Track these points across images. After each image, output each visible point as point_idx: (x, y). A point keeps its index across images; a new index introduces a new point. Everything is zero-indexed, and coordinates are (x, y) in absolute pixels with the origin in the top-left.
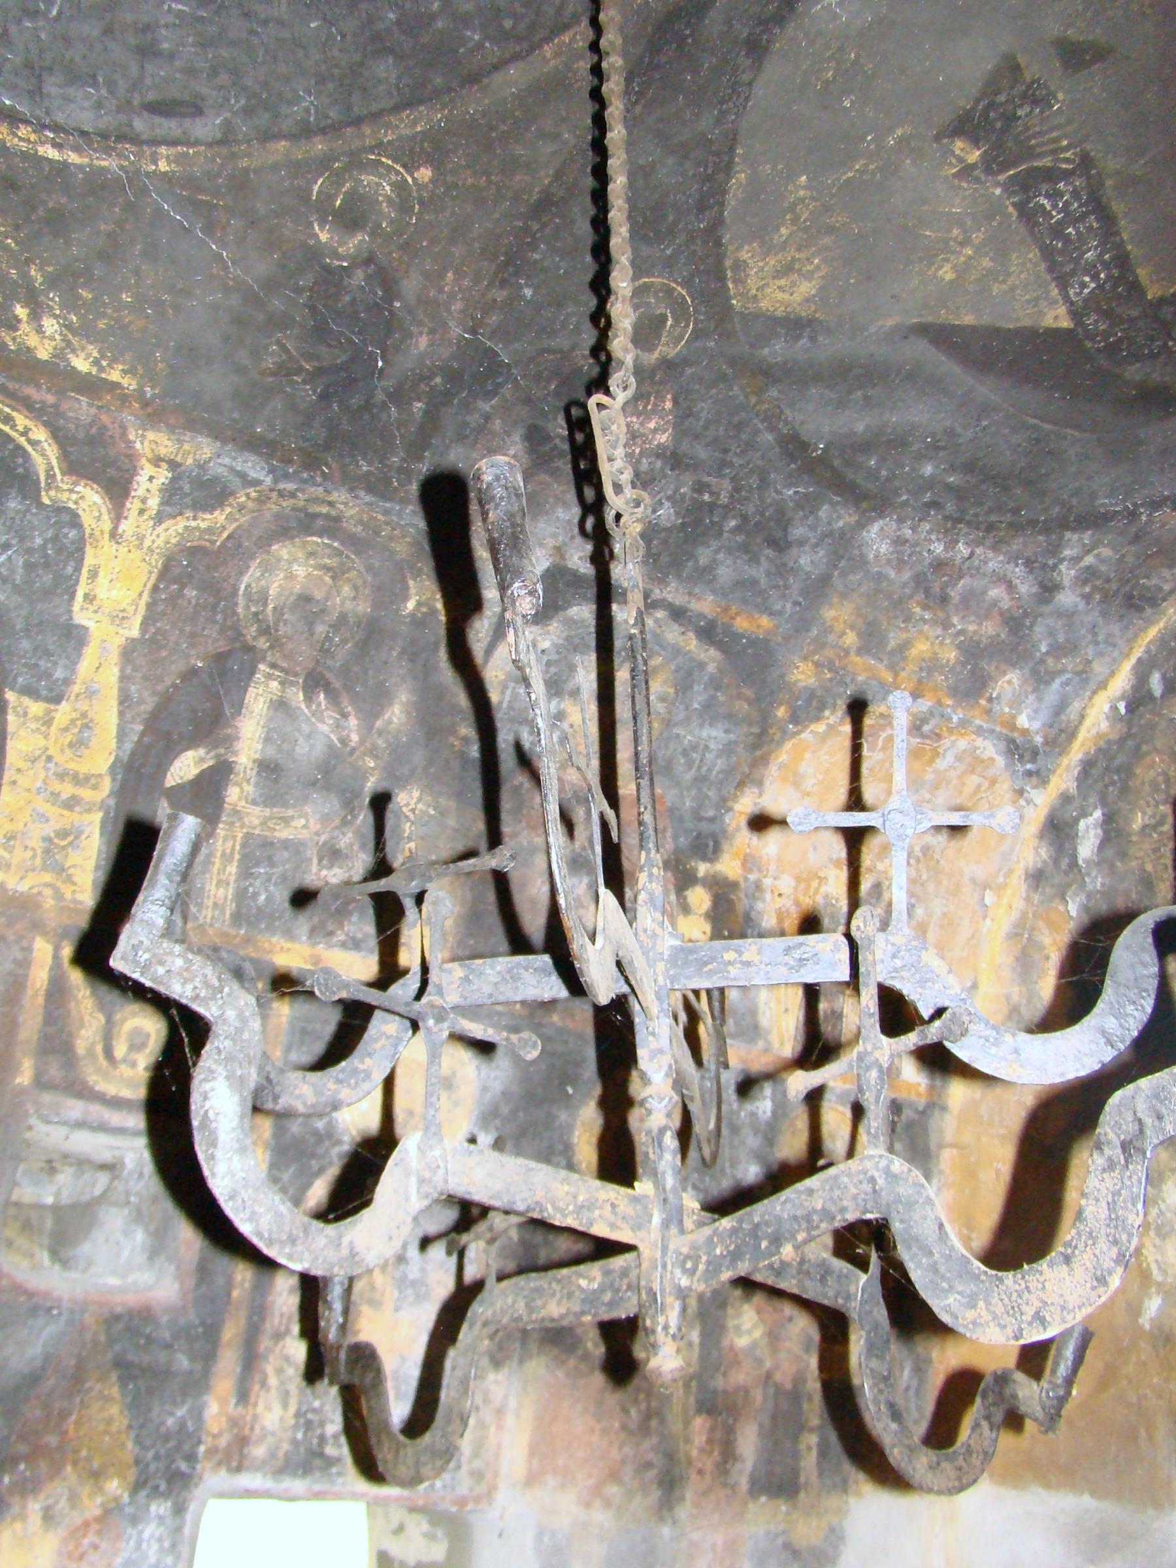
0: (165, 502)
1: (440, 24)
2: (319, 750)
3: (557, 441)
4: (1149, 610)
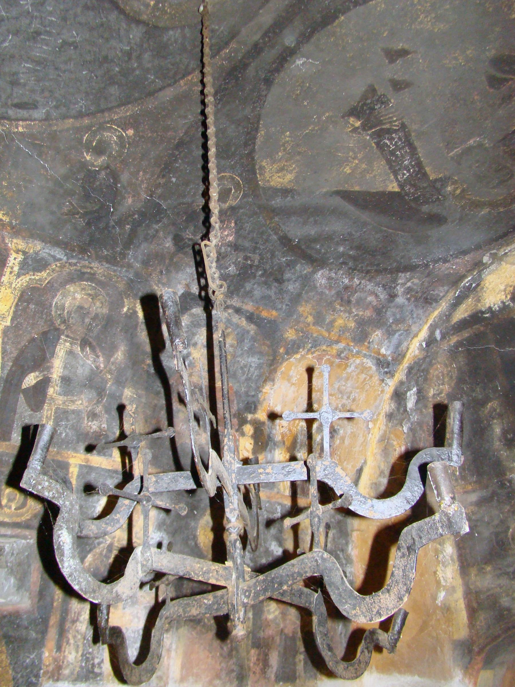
0: (21, 269)
1: (137, 72)
2: (87, 371)
3: (186, 240)
4: (434, 304)
